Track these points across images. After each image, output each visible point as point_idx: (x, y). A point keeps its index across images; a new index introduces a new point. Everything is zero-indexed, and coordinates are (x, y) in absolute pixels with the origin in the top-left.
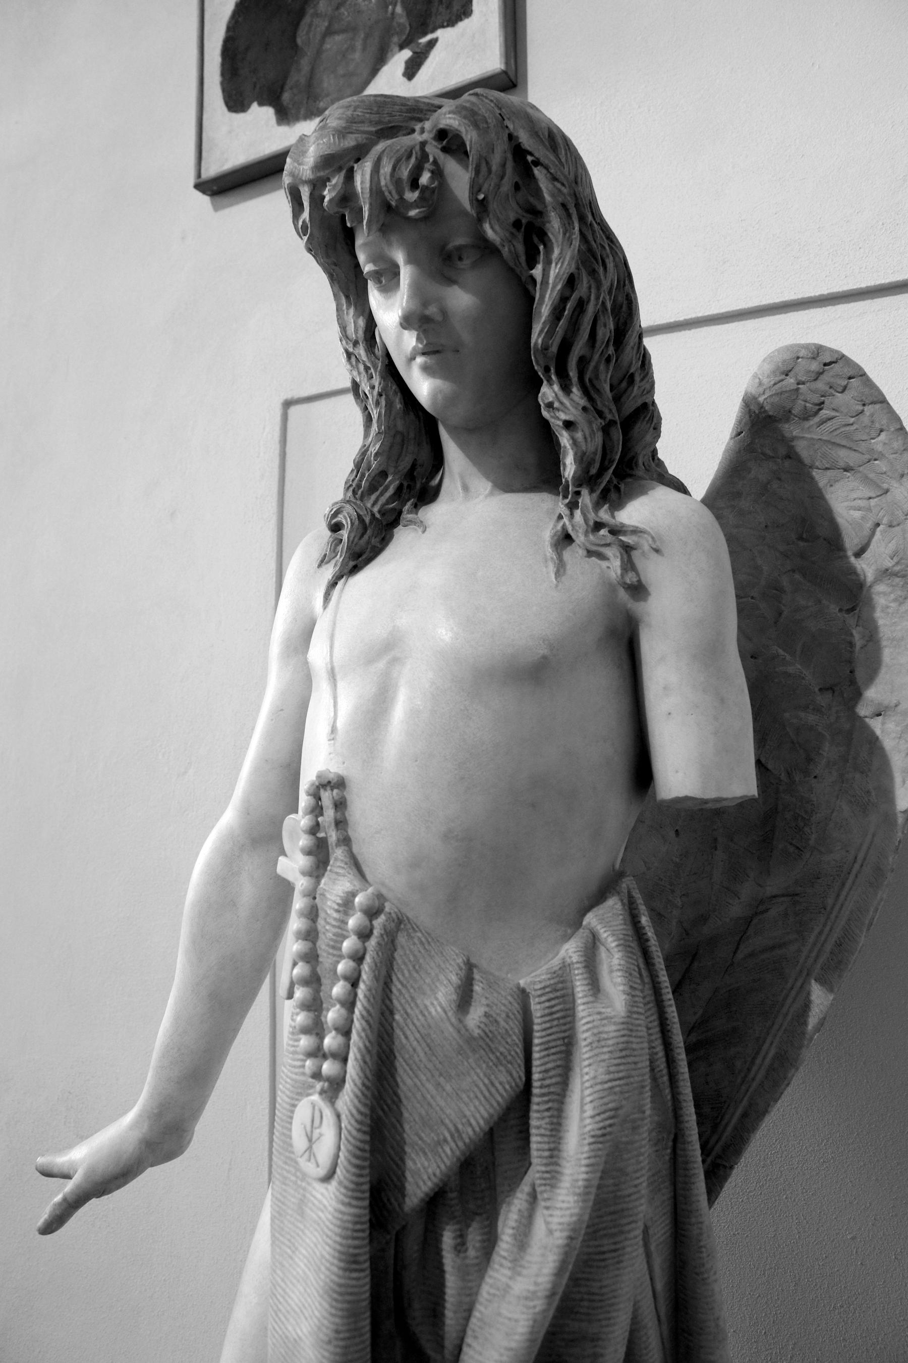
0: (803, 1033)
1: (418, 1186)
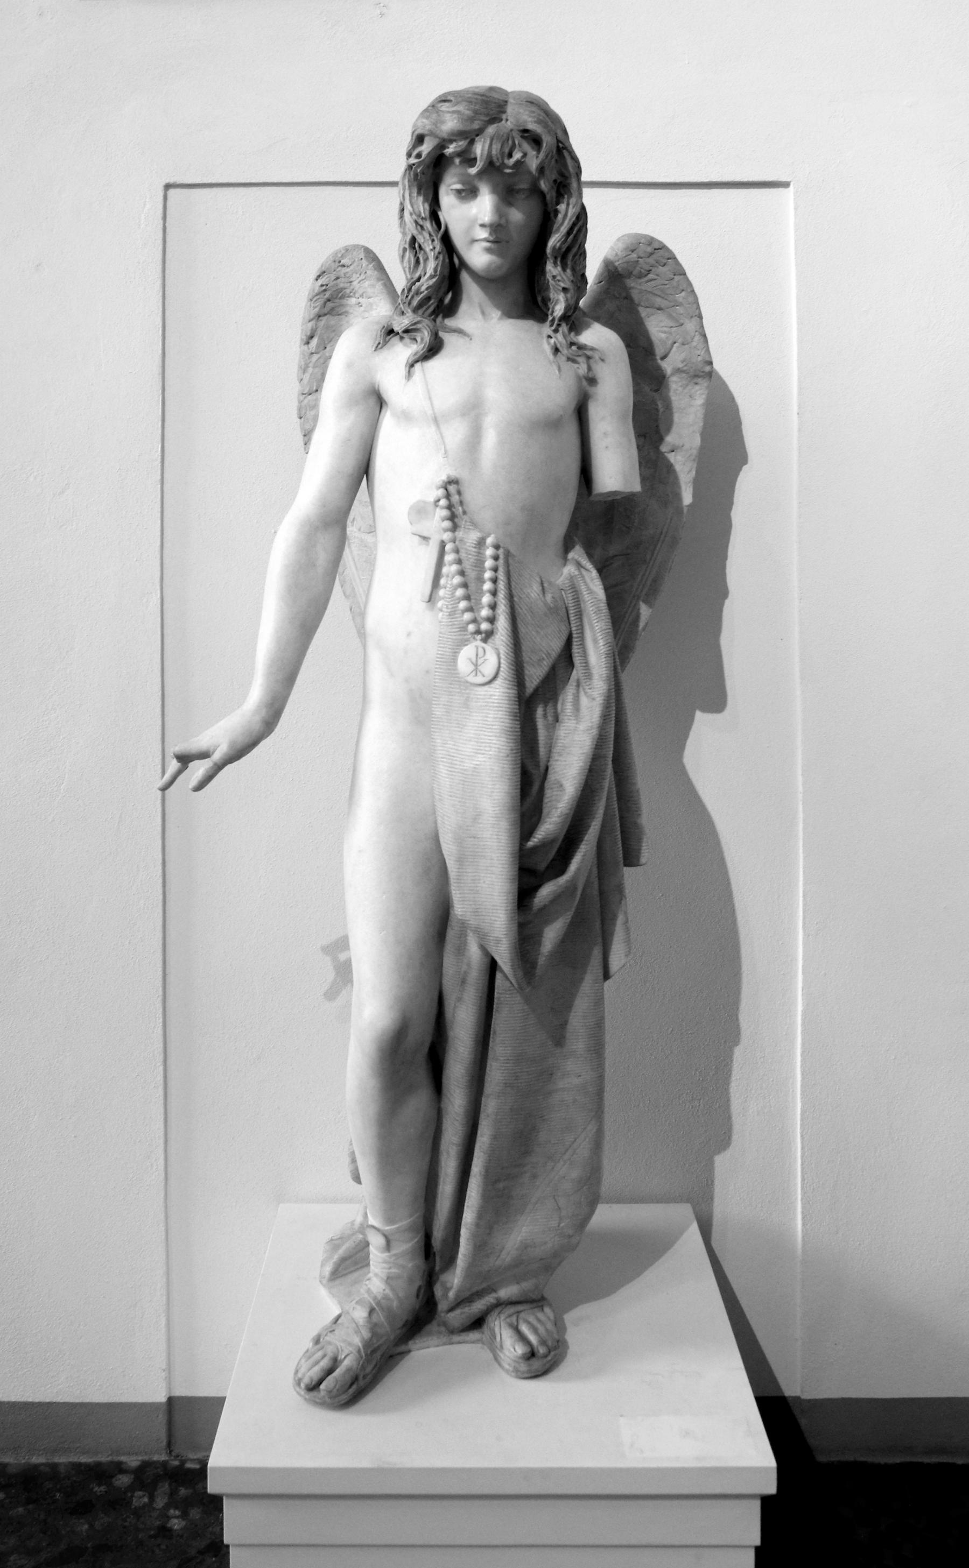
0: (637, 632)
1: (532, 683)
